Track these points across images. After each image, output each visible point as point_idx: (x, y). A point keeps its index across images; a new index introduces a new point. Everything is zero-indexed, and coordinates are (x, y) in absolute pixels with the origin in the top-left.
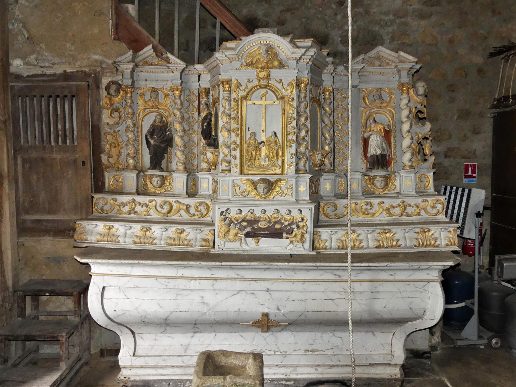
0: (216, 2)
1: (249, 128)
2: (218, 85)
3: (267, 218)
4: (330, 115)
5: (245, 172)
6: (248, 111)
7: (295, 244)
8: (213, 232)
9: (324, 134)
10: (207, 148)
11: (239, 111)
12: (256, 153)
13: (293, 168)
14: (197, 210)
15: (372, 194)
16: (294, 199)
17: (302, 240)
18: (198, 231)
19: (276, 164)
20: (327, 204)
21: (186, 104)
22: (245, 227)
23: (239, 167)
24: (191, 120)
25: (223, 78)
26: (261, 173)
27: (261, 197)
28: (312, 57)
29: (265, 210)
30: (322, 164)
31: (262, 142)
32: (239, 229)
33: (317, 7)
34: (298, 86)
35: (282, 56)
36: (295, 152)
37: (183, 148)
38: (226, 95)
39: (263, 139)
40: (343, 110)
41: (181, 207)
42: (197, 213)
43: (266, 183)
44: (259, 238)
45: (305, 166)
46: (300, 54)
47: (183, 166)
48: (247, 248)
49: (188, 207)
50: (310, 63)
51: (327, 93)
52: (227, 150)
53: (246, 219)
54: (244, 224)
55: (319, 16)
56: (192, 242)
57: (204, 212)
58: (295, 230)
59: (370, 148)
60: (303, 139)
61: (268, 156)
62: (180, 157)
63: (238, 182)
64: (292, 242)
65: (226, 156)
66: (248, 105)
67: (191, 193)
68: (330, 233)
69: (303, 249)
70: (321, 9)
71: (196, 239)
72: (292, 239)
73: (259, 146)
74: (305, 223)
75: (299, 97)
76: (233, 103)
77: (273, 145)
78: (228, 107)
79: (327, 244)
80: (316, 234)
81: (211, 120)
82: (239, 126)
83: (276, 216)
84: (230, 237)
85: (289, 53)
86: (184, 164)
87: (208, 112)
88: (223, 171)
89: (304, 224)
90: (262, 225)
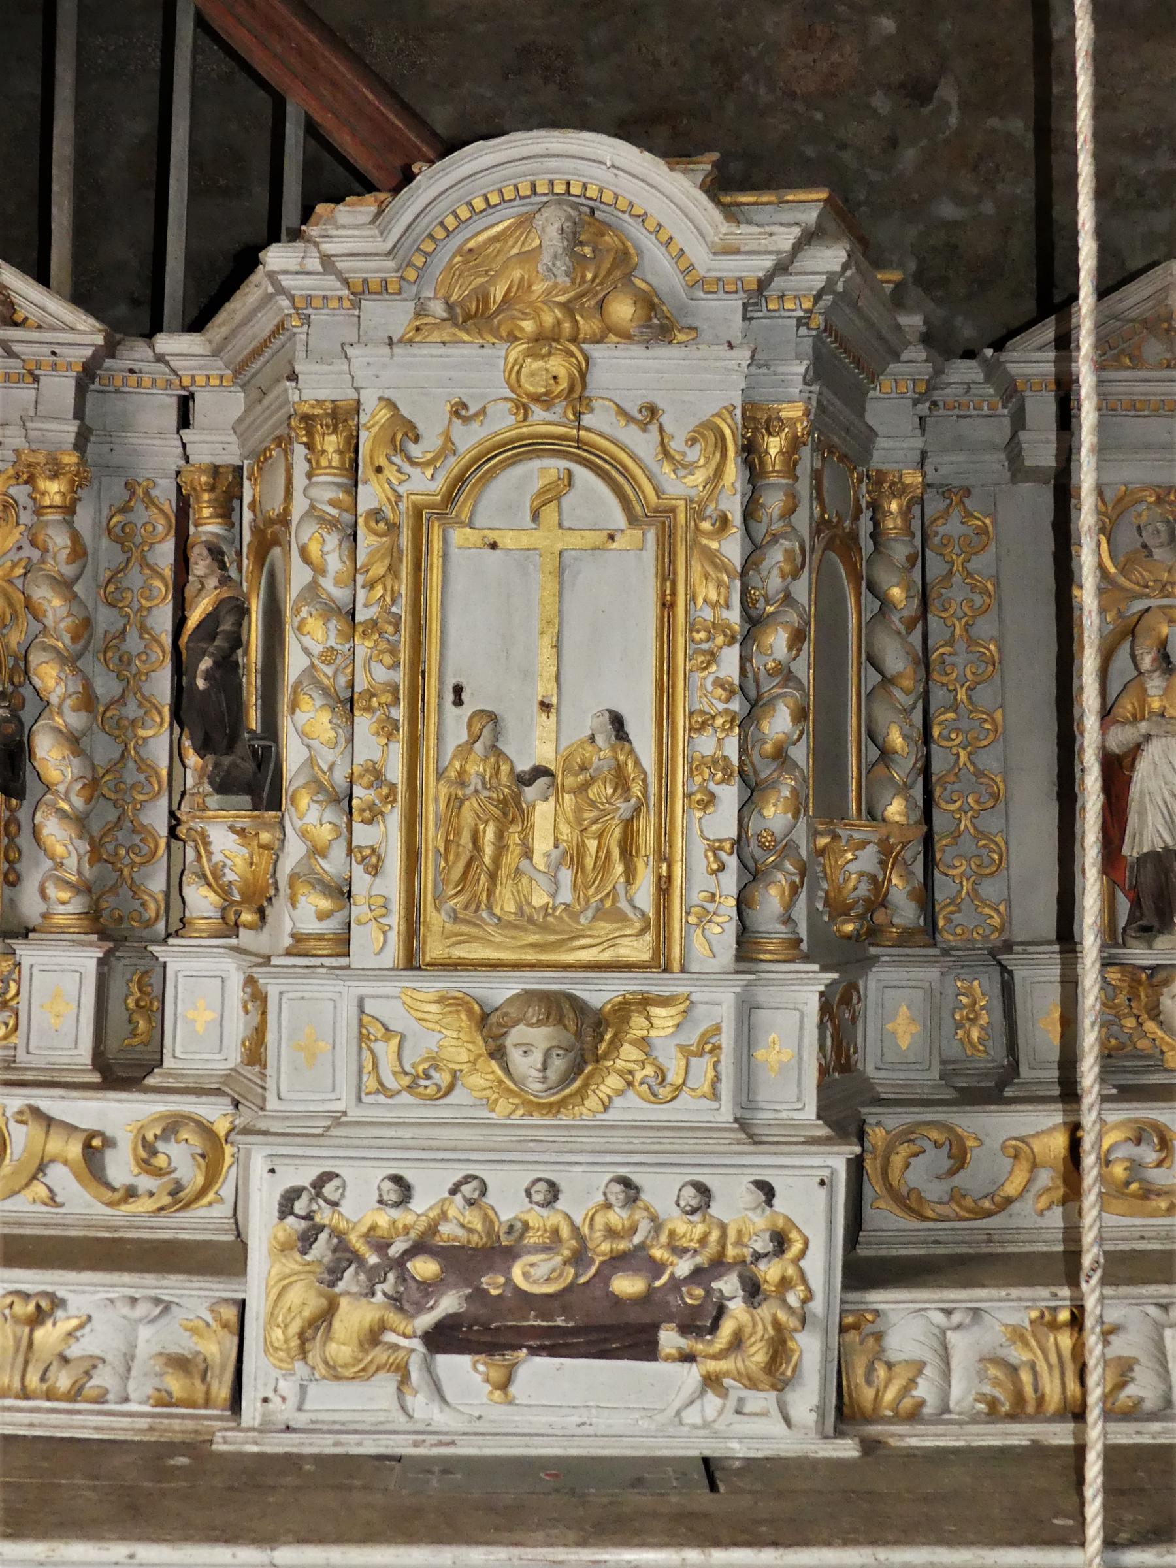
0: (285, 14)
1: (458, 690)
2: (284, 442)
3: (565, 1232)
4: (910, 625)
5: (434, 949)
6: (458, 585)
7: (734, 1395)
8: (230, 1314)
9: (880, 730)
10: (214, 800)
11: (404, 588)
12: (500, 835)
13: (722, 932)
14: (146, 1165)
15: (1147, 1070)
16: (725, 1113)
17: (778, 1369)
18: (142, 1309)
19: (623, 904)
20: (906, 1135)
21: (106, 553)
22: (429, 1289)
23: (395, 919)
24: (133, 643)
25: (308, 394)
26: (530, 956)
27: (533, 1107)
28: (832, 278)
29: (552, 1185)
30: (878, 899)
31: (540, 772)
32: (396, 1301)
33: (800, 107)
34: (750, 451)
35: (659, 271)
36: (734, 835)
37: (79, 802)
38: (327, 493)
39: (544, 753)
40: (978, 600)
41: (55, 1145)
42: (145, 1183)
43: (560, 1021)
44: (510, 1356)
45: (788, 920)
46: (768, 262)
47: (77, 905)
48: (440, 1418)
49: (94, 1149)
50: (818, 321)
51: (894, 506)
52: (330, 814)
53: (438, 1241)
54: (424, 1268)
55: (810, 152)
56: (103, 1379)
57: (190, 1174)
58: (737, 1307)
59: (1142, 814)
60: (780, 755)
61: (575, 858)
62: (60, 850)
63: (393, 1012)
64: (711, 1382)
65: (317, 851)
66: (454, 552)
67: (123, 1064)
68: (939, 1318)
69: (779, 1427)
70: (819, 116)
71: (129, 1359)
72: (712, 1366)
73: (517, 798)
74: (796, 1261)
75: (750, 512)
76: (367, 541)
77: (601, 791)
78: (335, 563)
79: (924, 1390)
80: (856, 1327)
81: (237, 641)
82: (401, 677)
83: (617, 1217)
84: (332, 1347)
85: (703, 260)
86: (84, 888)
87: (226, 593)
88: (300, 945)
89: (791, 1271)
90: (534, 1274)
